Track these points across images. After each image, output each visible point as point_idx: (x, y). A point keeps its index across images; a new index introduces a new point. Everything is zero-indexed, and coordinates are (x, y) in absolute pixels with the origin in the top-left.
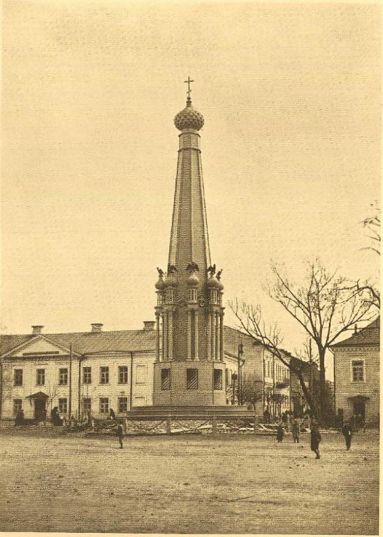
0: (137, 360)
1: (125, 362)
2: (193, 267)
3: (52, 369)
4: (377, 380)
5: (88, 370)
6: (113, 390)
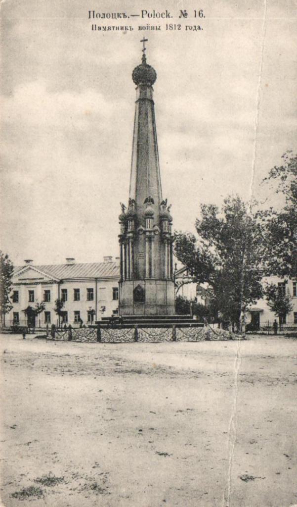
1: (92, 285)
2: (149, 201)
3: (39, 292)
5: (65, 291)
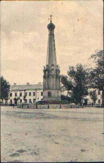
2: (53, 65)
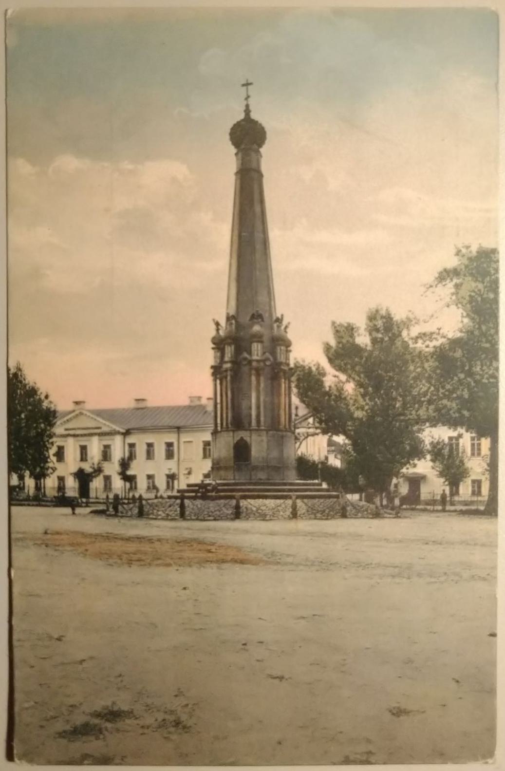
0: (185, 437)
4: (139, 758)
6: (160, 468)
